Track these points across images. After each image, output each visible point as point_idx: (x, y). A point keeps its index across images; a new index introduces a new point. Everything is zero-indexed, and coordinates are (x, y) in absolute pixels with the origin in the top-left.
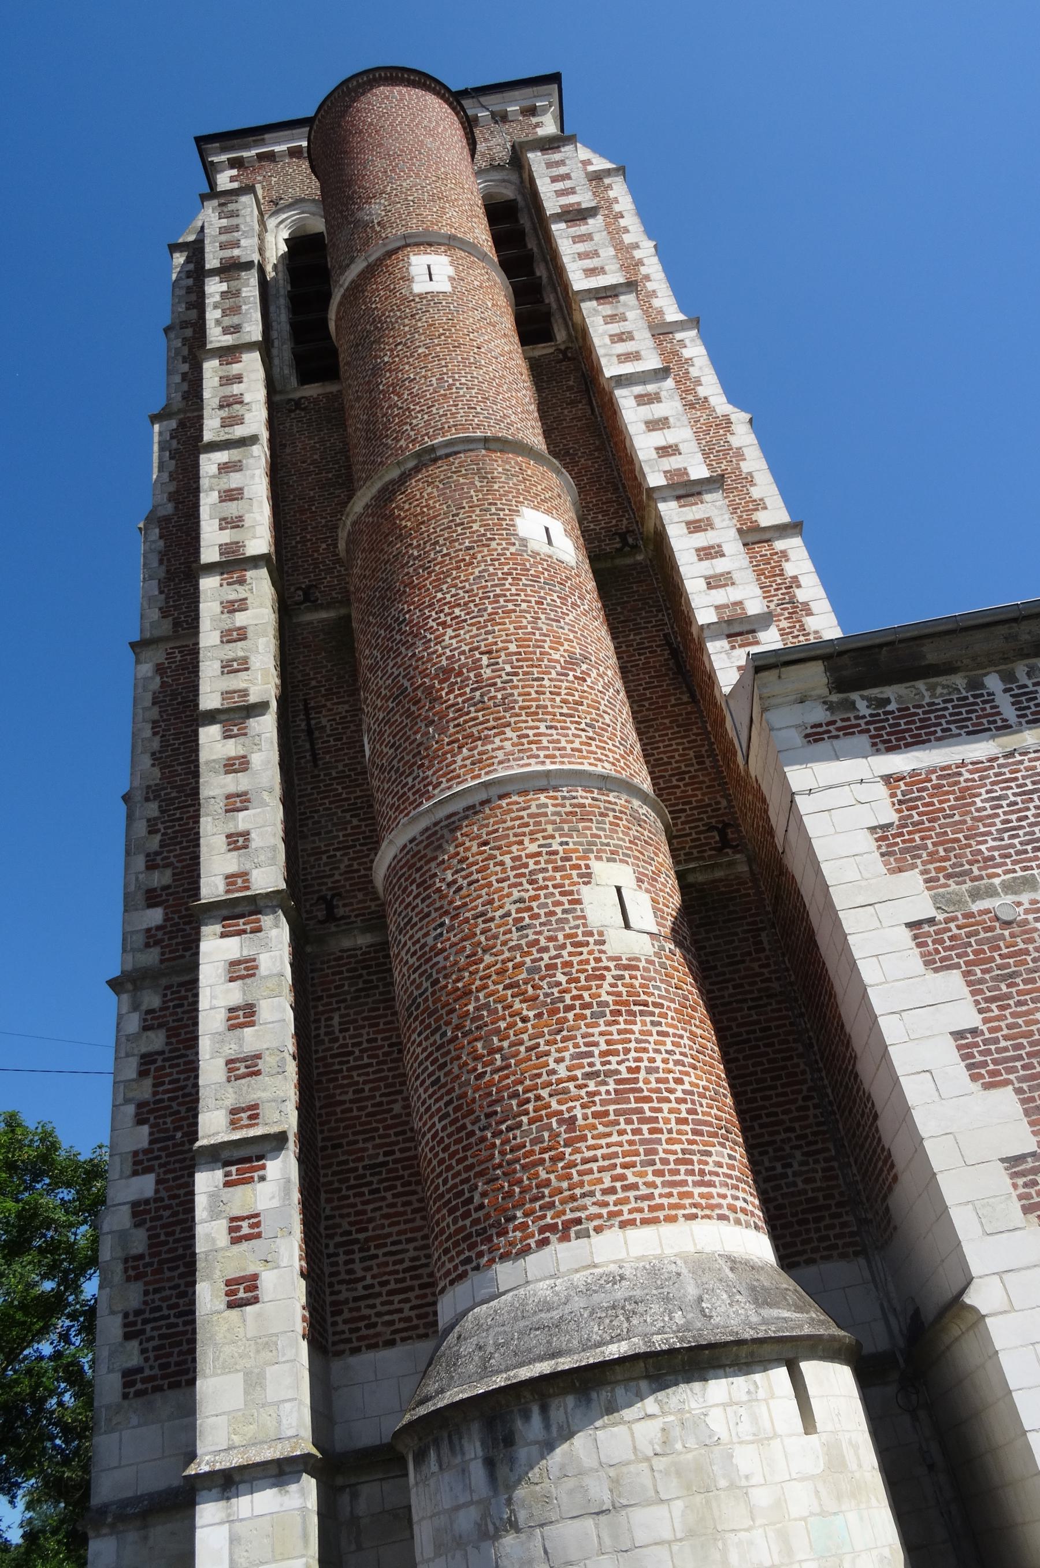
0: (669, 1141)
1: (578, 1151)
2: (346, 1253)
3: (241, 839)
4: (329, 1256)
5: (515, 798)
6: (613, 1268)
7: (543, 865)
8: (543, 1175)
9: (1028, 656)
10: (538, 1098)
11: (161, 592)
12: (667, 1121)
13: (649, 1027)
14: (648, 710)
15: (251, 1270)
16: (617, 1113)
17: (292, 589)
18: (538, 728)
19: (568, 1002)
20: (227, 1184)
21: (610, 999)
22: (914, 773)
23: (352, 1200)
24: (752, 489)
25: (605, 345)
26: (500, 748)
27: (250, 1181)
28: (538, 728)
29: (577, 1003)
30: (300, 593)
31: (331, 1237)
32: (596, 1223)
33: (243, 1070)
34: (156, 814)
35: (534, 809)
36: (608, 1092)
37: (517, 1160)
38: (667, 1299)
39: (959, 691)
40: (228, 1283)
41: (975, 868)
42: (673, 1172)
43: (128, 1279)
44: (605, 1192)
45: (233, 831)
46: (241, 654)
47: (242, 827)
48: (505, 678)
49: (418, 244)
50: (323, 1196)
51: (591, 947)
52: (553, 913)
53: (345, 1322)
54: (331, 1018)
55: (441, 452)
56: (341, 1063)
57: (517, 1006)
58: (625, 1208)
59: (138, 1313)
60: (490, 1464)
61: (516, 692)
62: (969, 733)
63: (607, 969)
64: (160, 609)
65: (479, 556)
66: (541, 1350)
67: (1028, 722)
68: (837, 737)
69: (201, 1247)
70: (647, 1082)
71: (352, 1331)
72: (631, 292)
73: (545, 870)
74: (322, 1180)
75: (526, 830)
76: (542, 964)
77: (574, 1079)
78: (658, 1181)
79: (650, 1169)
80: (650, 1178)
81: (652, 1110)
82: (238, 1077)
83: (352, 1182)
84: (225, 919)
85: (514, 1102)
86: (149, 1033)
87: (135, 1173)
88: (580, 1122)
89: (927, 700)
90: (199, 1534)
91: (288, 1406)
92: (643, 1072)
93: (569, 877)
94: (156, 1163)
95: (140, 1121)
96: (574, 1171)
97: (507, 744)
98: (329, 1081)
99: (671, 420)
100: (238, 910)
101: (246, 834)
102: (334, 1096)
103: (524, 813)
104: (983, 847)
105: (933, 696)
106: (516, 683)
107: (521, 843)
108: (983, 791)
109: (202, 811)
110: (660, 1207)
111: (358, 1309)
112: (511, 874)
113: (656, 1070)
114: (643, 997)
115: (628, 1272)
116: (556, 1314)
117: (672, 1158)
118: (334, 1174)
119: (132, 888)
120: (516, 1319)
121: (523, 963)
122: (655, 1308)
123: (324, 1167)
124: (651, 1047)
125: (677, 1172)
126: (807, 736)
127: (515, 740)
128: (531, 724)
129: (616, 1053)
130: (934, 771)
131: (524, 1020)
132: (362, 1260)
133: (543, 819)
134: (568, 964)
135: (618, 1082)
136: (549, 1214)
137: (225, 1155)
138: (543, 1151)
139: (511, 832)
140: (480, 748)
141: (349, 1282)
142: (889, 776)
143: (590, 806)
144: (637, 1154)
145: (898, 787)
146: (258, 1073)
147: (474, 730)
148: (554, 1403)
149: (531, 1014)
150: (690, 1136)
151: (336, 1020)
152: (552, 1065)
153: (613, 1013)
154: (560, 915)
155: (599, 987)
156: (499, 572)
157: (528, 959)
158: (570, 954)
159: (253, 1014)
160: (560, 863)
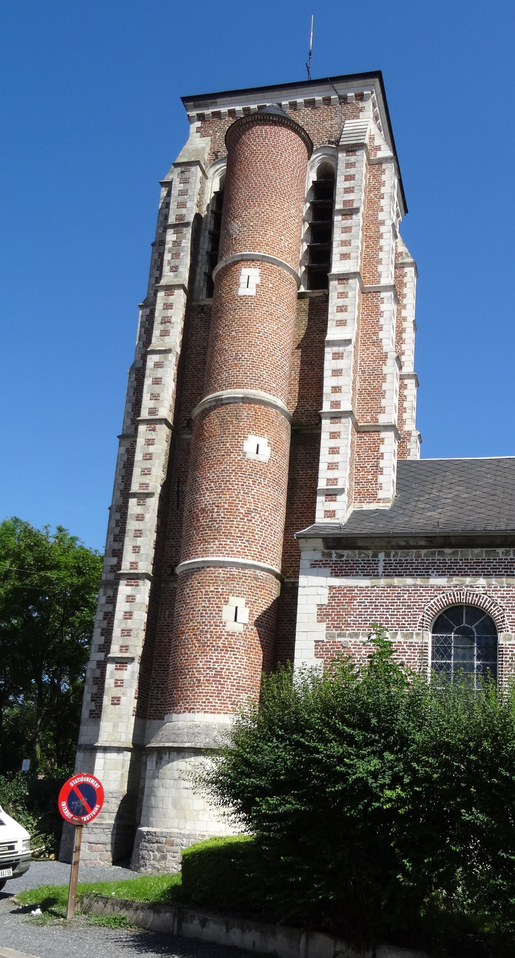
0: (226, 691)
1: (198, 689)
2: (157, 690)
3: (137, 549)
4: (152, 690)
5: (212, 569)
6: (198, 723)
7: (214, 596)
8: (189, 694)
9: (395, 549)
10: (193, 671)
11: (132, 411)
12: (228, 685)
13: (232, 656)
14: (305, 508)
15: (119, 695)
16: (213, 681)
17: (183, 419)
18: (226, 541)
19: (209, 644)
20: (116, 669)
21: (221, 645)
22: (340, 587)
23: (161, 675)
24: (383, 400)
25: (333, 313)
26: (212, 547)
27: (122, 669)
28: (226, 541)
29: (211, 645)
30: (186, 422)
31: (153, 684)
32: (198, 710)
33: (126, 634)
34: (119, 518)
35: (216, 575)
36: (212, 674)
37: (183, 687)
38: (207, 735)
39: (369, 556)
40: (112, 698)
41: (343, 626)
42: (224, 700)
43: (94, 684)
44: (203, 702)
45: (135, 545)
46: (149, 466)
47: (138, 544)
48: (221, 519)
49: (247, 260)
50: (153, 672)
51: (221, 627)
52: (212, 613)
53: (153, 710)
54: (165, 612)
55: (225, 402)
56: (166, 629)
57: (195, 642)
58: (207, 708)
59: (96, 694)
60: (157, 762)
61: (223, 526)
62: (364, 575)
63: (224, 635)
64: (131, 419)
65: (226, 460)
66: (172, 740)
67: (385, 575)
68: (321, 567)
69: (106, 686)
70: (225, 673)
71: (155, 713)
72: (355, 278)
73: (214, 598)
74: (154, 666)
75: (212, 582)
76: (204, 630)
77: (203, 668)
78: (219, 702)
79: (217, 698)
80: (217, 701)
81: (224, 681)
82: (124, 636)
83: (162, 669)
84: (128, 579)
85: (187, 671)
86: (108, 605)
87: (99, 652)
88: (202, 681)
89: (357, 558)
90: (97, 760)
91: (123, 734)
92: (225, 669)
93: (221, 601)
94: (105, 650)
95: (102, 635)
96: (196, 695)
97: (215, 546)
98: (161, 634)
99: (344, 371)
100: (132, 577)
101: (139, 547)
102: (162, 639)
103: (213, 575)
104: (349, 619)
105: (359, 557)
106: (223, 522)
107: (209, 586)
108: (358, 598)
109: (126, 535)
110: (217, 709)
111: (157, 707)
112: (204, 596)
113: (229, 669)
114: (233, 646)
115: (201, 725)
116: (180, 732)
117: (225, 696)
118: (158, 665)
119: (108, 548)
120: (172, 730)
121: (199, 628)
122: (203, 736)
123: (155, 662)
124: (230, 662)
125: (226, 700)
126: (311, 564)
127: (218, 545)
128: (225, 540)
129: (218, 663)
130: (346, 588)
131: (195, 647)
132: (161, 693)
133: (218, 579)
134: (212, 632)
135: (216, 671)
136: (188, 705)
137: (116, 660)
138: (190, 687)
139: (207, 581)
140: (206, 546)
141: (156, 699)
142: (332, 586)
143: (236, 575)
144: (215, 693)
145: (333, 591)
146: (130, 636)
147: (206, 538)
148: (172, 753)
149: (198, 645)
150: (234, 690)
151: (167, 613)
152: (199, 663)
153: (221, 650)
154: (214, 615)
155: (219, 641)
156: (231, 469)
157: (201, 627)
158: (214, 629)
159: (131, 615)
160: (219, 596)
